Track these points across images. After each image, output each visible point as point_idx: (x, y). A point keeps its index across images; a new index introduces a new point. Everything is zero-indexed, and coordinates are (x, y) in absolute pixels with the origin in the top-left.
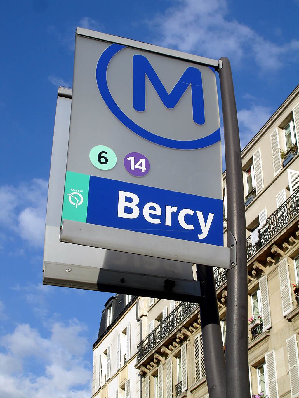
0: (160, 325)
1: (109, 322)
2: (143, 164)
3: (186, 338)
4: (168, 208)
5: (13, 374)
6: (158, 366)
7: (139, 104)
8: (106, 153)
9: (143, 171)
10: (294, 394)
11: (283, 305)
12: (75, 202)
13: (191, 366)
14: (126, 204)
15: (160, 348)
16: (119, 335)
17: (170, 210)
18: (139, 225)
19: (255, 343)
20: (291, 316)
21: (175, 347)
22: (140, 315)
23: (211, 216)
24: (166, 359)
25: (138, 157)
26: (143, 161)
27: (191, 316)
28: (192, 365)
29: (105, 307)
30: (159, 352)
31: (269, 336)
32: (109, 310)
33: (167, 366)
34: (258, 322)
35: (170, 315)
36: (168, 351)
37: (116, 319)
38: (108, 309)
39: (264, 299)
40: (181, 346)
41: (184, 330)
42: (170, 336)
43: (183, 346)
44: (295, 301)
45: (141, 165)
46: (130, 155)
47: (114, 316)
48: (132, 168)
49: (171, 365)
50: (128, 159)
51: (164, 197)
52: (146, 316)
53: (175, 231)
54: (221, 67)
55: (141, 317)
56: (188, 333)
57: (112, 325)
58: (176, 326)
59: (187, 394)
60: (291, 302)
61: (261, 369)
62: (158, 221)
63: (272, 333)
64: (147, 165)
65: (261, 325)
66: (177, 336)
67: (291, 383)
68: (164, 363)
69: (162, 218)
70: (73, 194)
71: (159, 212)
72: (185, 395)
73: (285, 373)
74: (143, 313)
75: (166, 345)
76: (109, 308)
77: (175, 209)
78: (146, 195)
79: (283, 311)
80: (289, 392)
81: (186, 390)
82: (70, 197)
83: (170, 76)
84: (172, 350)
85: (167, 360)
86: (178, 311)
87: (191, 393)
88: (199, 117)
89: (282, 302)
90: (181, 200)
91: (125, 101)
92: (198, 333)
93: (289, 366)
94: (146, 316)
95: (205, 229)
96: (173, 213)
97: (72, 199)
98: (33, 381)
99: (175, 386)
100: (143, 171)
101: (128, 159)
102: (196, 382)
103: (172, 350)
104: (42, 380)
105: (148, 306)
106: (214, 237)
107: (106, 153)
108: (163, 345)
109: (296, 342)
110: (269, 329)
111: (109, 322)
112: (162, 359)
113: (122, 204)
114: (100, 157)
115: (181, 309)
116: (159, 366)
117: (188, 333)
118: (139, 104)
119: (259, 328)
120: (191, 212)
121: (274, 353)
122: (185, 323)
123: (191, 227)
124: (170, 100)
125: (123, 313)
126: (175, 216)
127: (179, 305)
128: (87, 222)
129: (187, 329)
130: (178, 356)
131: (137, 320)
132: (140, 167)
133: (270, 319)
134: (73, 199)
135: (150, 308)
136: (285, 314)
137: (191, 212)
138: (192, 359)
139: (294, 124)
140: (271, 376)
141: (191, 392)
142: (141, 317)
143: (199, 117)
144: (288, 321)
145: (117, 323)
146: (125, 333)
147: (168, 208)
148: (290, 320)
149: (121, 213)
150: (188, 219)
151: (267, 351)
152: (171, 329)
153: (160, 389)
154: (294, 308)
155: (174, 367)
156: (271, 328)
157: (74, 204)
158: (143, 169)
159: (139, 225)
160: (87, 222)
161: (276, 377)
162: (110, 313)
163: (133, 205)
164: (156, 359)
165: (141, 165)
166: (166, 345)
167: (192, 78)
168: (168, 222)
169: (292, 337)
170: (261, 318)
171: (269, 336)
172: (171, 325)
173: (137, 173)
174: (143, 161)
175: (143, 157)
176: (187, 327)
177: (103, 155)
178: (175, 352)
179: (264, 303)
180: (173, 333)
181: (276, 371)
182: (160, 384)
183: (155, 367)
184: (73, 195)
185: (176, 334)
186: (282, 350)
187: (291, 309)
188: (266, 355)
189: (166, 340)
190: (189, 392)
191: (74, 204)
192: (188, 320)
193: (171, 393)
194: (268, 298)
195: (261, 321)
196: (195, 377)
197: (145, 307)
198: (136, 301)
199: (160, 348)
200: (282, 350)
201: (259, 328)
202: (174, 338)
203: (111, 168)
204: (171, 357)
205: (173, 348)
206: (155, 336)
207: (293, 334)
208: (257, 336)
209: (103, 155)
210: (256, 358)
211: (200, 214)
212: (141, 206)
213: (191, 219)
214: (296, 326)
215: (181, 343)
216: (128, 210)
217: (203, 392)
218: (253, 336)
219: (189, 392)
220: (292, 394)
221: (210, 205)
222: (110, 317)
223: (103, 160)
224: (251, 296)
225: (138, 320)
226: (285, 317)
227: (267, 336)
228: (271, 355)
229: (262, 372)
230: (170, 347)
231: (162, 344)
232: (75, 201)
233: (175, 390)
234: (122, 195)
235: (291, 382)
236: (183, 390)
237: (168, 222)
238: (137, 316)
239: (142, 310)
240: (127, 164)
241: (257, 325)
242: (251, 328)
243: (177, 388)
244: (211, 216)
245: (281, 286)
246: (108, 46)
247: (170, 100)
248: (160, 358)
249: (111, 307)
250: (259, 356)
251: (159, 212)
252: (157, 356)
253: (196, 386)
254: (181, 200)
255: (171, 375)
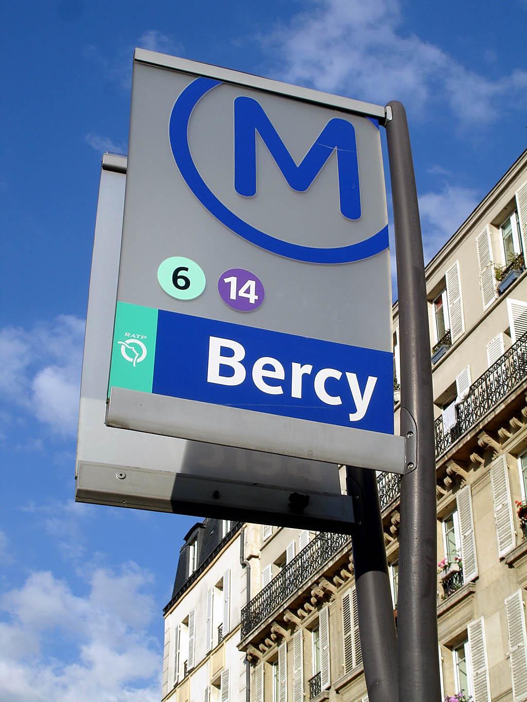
0: (283, 574)
1: (192, 568)
2: (253, 290)
3: (327, 596)
4: (296, 366)
5: (23, 660)
6: (278, 645)
7: (246, 184)
8: (186, 269)
9: (252, 301)
10: (518, 695)
11: (499, 538)
12: (133, 356)
13: (336, 646)
14: (223, 360)
15: (282, 614)
16: (210, 590)
17: (299, 371)
18: (246, 397)
19: (449, 604)
20: (512, 558)
21: (309, 611)
22: (246, 556)
23: (372, 381)
24: (292, 633)
25: (243, 277)
26: (251, 284)
27: (337, 558)
28: (339, 644)
29: (185, 542)
30: (280, 621)
31: (473, 592)
32: (192, 547)
33: (294, 645)
34: (455, 567)
35: (300, 556)
36: (296, 619)
37: (205, 562)
38: (190, 545)
39: (465, 528)
40: (318, 610)
41: (325, 583)
42: (300, 593)
43: (322, 611)
44: (521, 531)
45: (248, 291)
46: (229, 274)
47: (200, 557)
48: (233, 296)
49: (302, 644)
50: (226, 280)
51: (288, 348)
52: (258, 557)
53: (308, 408)
54: (390, 117)
55: (249, 559)
56: (331, 587)
57: (197, 574)
58: (311, 574)
59: (330, 695)
60: (513, 532)
61: (460, 650)
62: (278, 391)
63: (480, 587)
64: (260, 290)
65: (460, 573)
66: (312, 592)
67: (513, 676)
68: (288, 640)
69: (286, 384)
70: (129, 341)
71: (279, 374)
72: (326, 696)
73: (503, 658)
74: (253, 552)
75: (293, 609)
76: (192, 544)
77: (308, 369)
78: (258, 344)
79: (499, 549)
80: (510, 691)
81: (329, 689)
82: (123, 348)
83: (300, 134)
84: (303, 617)
85: (295, 634)
86: (315, 548)
87: (337, 692)
88: (351, 206)
89: (498, 533)
90: (318, 353)
91: (220, 178)
92: (348, 588)
93: (510, 645)
94: (258, 557)
95: (362, 404)
96: (305, 376)
97: (127, 350)
98: (58, 672)
99: (309, 681)
100: (252, 301)
101: (226, 280)
102: (345, 674)
103: (303, 617)
104: (73, 670)
105: (261, 541)
106: (378, 419)
107: (186, 269)
108: (287, 608)
109: (522, 603)
110: (474, 581)
111: (192, 568)
112: (286, 633)
113: (215, 360)
114: (175, 277)
115: (319, 545)
116: (281, 646)
117: (331, 587)
118: (246, 184)
119: (456, 579)
120: (337, 375)
121: (483, 623)
122: (326, 569)
123: (336, 401)
124: (300, 177)
125: (216, 552)
126: (308, 381)
127: (315, 538)
128: (153, 392)
129: (330, 580)
130: (314, 627)
131: (242, 564)
132: (246, 295)
133: (476, 563)
134: (128, 352)
135: (265, 543)
136: (502, 554)
137: (337, 375)
138: (339, 633)
139: (517, 218)
140: (478, 663)
141: (337, 691)
142: (249, 559)
143: (351, 206)
144: (507, 566)
145: (206, 570)
146: (221, 588)
147: (296, 366)
148: (511, 565)
149: (213, 376)
150: (332, 386)
151: (470, 619)
152: (302, 580)
153: (283, 687)
154: (519, 544)
155: (307, 648)
156: (477, 578)
157: (131, 360)
158: (253, 298)
159: (246, 397)
160: (153, 392)
161: (487, 665)
162: (193, 552)
163: (234, 362)
164: (276, 633)
165: (248, 291)
166: (293, 609)
167: (338, 137)
168: (297, 392)
169: (515, 594)
170: (460, 561)
171: (473, 592)
172: (302, 573)
173: (241, 304)
174: (251, 284)
175: (253, 278)
176: (329, 576)
177: (181, 273)
178: (308, 621)
179: (466, 534)
180: (305, 588)
181: (486, 655)
182: (283, 678)
183: (274, 648)
184: (129, 345)
185: (309, 589)
186: (496, 617)
187: (513, 545)
188: (469, 626)
189: (293, 599)
190: (333, 692)
191: (131, 360)
192: (331, 564)
193: (302, 694)
194: (472, 526)
195: (461, 567)
196: (344, 665)
197: (255, 542)
198: (240, 531)
199: (282, 614)
200: (496, 617)
201: (456, 579)
202: (306, 597)
203: (195, 296)
204: (301, 629)
205: (305, 614)
206: (273, 593)
207: (517, 589)
208: (453, 593)
209: (181, 273)
210: (451, 632)
211: (352, 378)
212: (248, 363)
213: (337, 387)
214: (522, 575)
215: (319, 604)
216: (226, 371)
217: (358, 691)
218: (446, 592)
219: (333, 692)
220: (514, 694)
221: (369, 362)
222: (194, 559)
223: (181, 282)
224: (442, 522)
225: (244, 565)
226: (502, 559)
227: (471, 593)
228: (478, 626)
229: (462, 655)
230: (300, 612)
231: (286, 606)
232: (132, 355)
233: (308, 687)
234: (216, 344)
235: (512, 673)
236: (323, 688)
237: (297, 392)
238: (242, 557)
239: (250, 547)
240: (224, 289)
241: (454, 573)
242: (443, 579)
243: (311, 685)
244: (372, 381)
245: (495, 505)
246: (191, 81)
247: (300, 177)
248: (282, 631)
249: (196, 542)
250: (457, 628)
251: (279, 374)
252: (276, 627)
253: (345, 681)
254: (318, 353)
255: (302, 662)
